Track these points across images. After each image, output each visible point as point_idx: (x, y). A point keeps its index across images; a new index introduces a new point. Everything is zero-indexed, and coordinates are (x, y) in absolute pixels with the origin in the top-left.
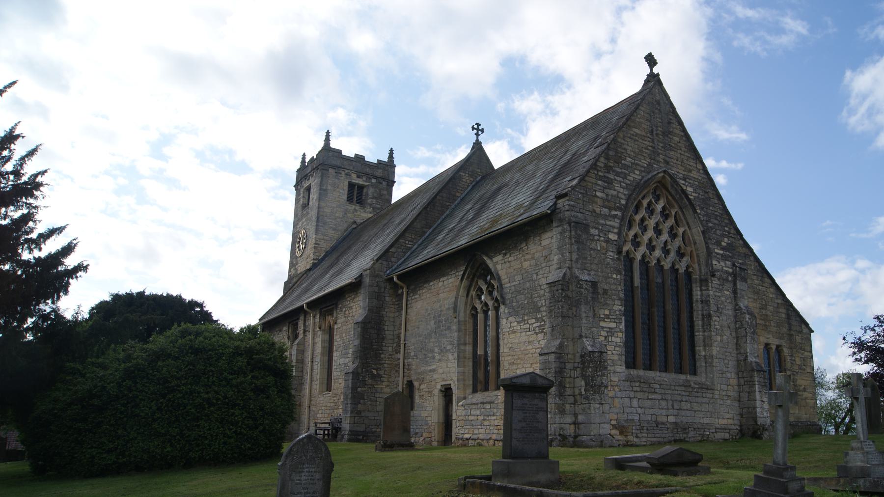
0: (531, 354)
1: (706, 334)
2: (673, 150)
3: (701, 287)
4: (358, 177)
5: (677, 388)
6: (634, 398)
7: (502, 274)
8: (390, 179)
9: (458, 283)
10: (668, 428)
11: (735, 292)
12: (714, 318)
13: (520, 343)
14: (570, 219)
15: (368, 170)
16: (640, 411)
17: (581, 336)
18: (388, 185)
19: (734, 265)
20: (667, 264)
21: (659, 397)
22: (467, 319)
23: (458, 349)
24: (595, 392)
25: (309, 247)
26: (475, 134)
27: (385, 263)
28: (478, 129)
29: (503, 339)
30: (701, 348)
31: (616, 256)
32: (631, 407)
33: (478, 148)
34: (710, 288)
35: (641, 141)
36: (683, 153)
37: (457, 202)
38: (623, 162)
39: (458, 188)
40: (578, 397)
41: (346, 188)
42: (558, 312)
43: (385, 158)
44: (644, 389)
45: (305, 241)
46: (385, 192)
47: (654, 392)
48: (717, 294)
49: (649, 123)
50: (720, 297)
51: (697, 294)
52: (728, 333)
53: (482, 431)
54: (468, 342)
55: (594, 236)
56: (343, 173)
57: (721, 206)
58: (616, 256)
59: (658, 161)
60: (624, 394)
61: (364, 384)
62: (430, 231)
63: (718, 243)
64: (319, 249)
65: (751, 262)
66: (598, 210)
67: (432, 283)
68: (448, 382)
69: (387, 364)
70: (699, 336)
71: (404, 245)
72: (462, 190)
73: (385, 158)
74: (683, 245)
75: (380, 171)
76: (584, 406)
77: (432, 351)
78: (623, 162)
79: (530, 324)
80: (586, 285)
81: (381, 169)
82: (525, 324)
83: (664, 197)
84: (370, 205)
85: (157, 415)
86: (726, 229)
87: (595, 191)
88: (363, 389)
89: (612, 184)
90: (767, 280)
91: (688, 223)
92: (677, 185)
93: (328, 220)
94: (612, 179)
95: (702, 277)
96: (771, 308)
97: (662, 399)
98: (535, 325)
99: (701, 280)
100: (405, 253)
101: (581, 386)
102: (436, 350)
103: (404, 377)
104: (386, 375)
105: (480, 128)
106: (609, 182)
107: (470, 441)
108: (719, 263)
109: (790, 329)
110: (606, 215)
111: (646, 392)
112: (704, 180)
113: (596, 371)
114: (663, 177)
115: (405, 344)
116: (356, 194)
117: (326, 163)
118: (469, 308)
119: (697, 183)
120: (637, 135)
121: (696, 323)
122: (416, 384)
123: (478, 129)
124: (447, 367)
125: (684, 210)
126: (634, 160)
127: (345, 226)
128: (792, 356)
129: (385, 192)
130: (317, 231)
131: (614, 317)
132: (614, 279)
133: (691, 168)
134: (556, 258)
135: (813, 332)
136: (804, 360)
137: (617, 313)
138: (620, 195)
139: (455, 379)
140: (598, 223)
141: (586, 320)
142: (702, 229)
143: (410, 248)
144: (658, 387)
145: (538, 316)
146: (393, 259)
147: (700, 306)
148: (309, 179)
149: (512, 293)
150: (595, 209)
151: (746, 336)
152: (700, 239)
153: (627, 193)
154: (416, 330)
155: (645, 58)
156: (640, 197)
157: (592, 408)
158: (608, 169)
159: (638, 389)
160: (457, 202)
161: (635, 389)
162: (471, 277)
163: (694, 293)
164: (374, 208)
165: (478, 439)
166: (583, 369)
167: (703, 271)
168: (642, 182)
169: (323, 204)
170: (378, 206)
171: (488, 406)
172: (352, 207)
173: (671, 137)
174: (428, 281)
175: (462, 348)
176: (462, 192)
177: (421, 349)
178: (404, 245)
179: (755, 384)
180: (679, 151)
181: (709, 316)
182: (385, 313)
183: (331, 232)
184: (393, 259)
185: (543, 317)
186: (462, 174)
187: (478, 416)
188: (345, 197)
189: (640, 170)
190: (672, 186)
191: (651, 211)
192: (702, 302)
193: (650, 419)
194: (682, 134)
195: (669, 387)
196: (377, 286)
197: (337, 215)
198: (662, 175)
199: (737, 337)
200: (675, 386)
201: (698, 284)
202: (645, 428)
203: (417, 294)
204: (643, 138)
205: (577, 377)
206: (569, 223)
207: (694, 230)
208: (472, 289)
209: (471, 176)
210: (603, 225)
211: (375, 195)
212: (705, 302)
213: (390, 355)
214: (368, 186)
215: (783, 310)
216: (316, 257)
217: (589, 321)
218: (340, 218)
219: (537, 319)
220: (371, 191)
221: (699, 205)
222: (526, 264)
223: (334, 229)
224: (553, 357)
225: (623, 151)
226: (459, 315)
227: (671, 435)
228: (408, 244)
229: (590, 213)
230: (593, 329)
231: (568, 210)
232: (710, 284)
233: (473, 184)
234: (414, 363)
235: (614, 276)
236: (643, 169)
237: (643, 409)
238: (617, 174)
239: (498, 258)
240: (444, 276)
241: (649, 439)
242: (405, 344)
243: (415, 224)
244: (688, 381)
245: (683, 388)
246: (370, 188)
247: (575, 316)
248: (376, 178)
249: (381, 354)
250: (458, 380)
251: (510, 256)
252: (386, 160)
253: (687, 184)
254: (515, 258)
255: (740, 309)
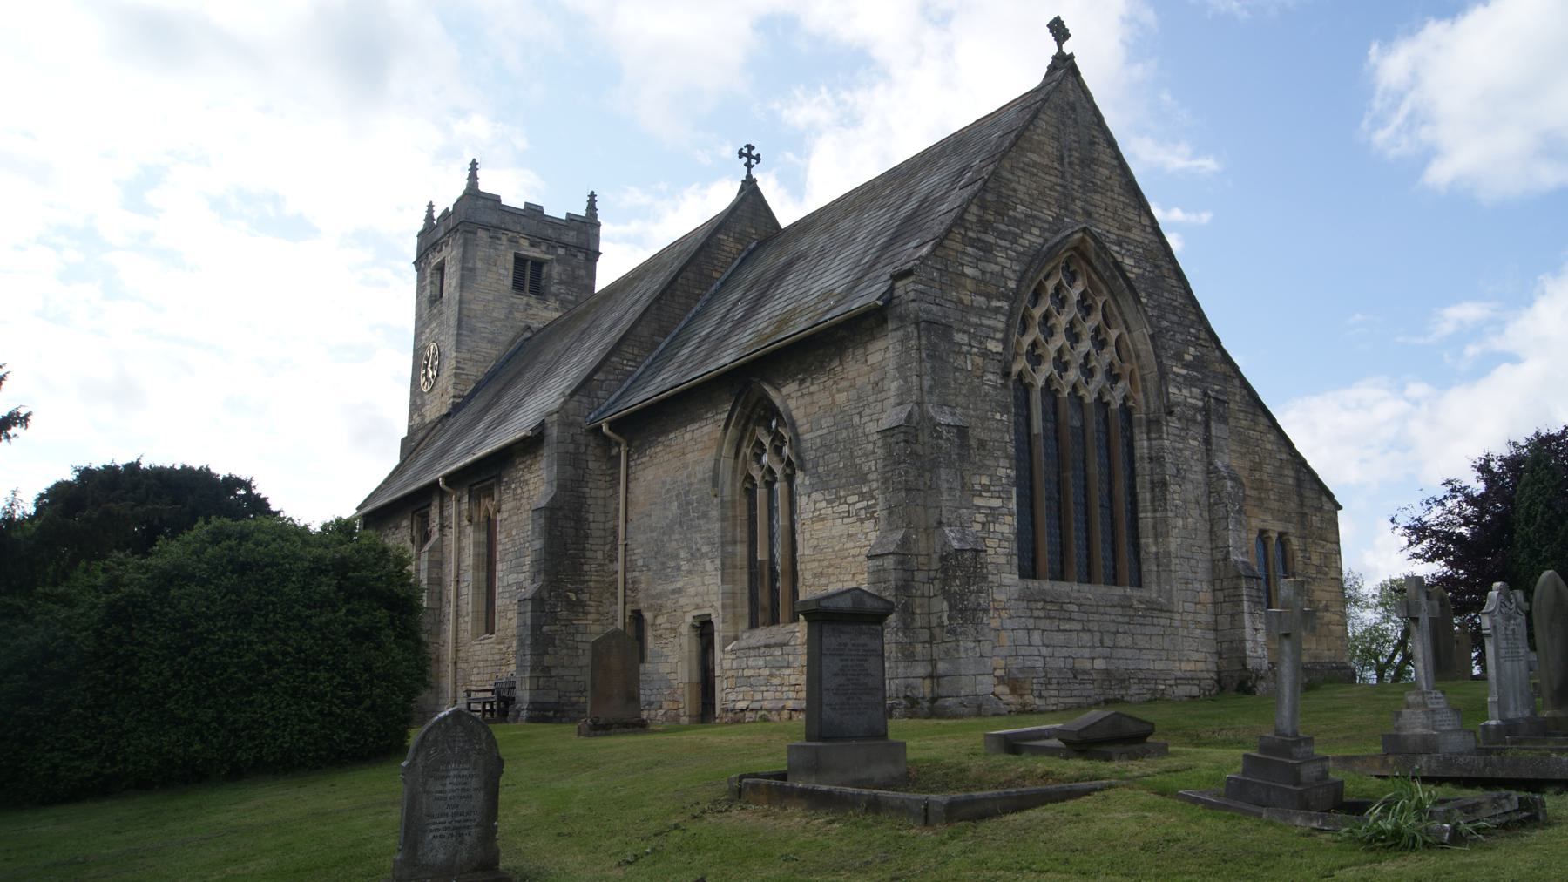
0: (853, 556)
1: (1158, 515)
2: (1099, 192)
3: (1148, 433)
4: (532, 245)
5: (1108, 610)
6: (1035, 629)
7: (798, 415)
8: (592, 248)
9: (719, 434)
10: (1093, 680)
11: (1207, 441)
12: (1172, 488)
13: (833, 538)
14: (917, 317)
15: (550, 232)
16: (1044, 651)
17: (940, 523)
18: (587, 259)
19: (1205, 394)
20: (1089, 395)
21: (1078, 626)
22: (737, 497)
23: (722, 551)
24: (965, 621)
25: (445, 375)
26: (745, 165)
27: (585, 400)
28: (749, 156)
29: (803, 532)
30: (1150, 540)
31: (999, 381)
32: (1030, 645)
33: (750, 190)
34: (1165, 436)
35: (1043, 175)
36: (1116, 196)
37: (713, 288)
38: (1011, 213)
39: (715, 262)
40: (937, 631)
41: (511, 266)
42: (900, 482)
43: (581, 211)
44: (1052, 614)
45: (437, 363)
46: (582, 272)
47: (1070, 619)
48: (1177, 445)
49: (1056, 144)
50: (1181, 450)
51: (1142, 445)
52: (1195, 512)
53: (768, 695)
54: (739, 539)
55: (961, 345)
56: (504, 238)
57: (1182, 291)
58: (999, 381)
59: (1073, 212)
60: (1016, 623)
61: (554, 618)
62: (667, 340)
63: (1178, 357)
64: (463, 376)
65: (1234, 388)
66: (967, 300)
67: (672, 435)
68: (706, 611)
69: (595, 581)
70: (1146, 518)
71: (620, 367)
72: (722, 267)
73: (581, 211)
74: (1116, 361)
75: (572, 233)
76: (948, 645)
77: (676, 557)
78: (1011, 213)
79: (849, 505)
80: (948, 432)
81: (573, 229)
82: (840, 504)
83: (1083, 275)
84: (556, 296)
85: (173, 686)
86: (1192, 330)
87: (962, 265)
88: (553, 628)
89: (991, 253)
90: (1264, 420)
91: (1125, 322)
92: (1106, 254)
93: (479, 325)
94: (991, 244)
95: (1151, 416)
96: (1269, 469)
97: (1083, 630)
98: (859, 506)
99: (1149, 422)
100: (622, 381)
101: (942, 611)
102: (683, 554)
103: (625, 604)
104: (594, 601)
105: (754, 153)
106: (988, 249)
107: (748, 714)
108: (1180, 390)
109: (1302, 505)
110: (982, 309)
111: (1054, 618)
112: (1154, 245)
113: (968, 583)
114: (1083, 240)
115: (626, 545)
116: (528, 277)
117: (473, 220)
118: (740, 478)
119: (1141, 250)
120: (1035, 164)
121: (1140, 497)
122: (648, 616)
123: (749, 156)
124: (704, 584)
125: (1119, 300)
126: (1031, 209)
127: (511, 334)
128: (1305, 550)
129: (582, 272)
130: (459, 344)
131: (997, 489)
132: (998, 421)
133: (1131, 223)
134: (894, 385)
135: (1340, 508)
136: (1326, 557)
137: (1004, 481)
138: (1006, 272)
139: (718, 604)
140: (968, 323)
141: (949, 495)
142: (1151, 332)
143: (631, 373)
144: (1075, 608)
145: (864, 490)
146: (600, 394)
147: (1147, 465)
148: (441, 250)
149: (816, 450)
150: (963, 297)
151: (1227, 518)
152: (1146, 348)
153: (1017, 268)
154: (645, 519)
155: (1048, 26)
156: (1042, 276)
157: (962, 649)
158: (985, 225)
159: (1042, 614)
160: (713, 288)
161: (1036, 613)
162: (743, 422)
163: (1137, 444)
164: (563, 302)
165: (761, 709)
166: (944, 582)
167: (1152, 406)
168: (1045, 248)
169: (467, 295)
170: (571, 298)
171: (778, 652)
172: (521, 300)
173: (1096, 167)
174: (665, 432)
175: (730, 549)
176: (723, 270)
177: (656, 553)
178: (620, 367)
179: (1242, 601)
180: (1109, 194)
181: (1164, 485)
182: (588, 490)
183: (484, 347)
184: (600, 394)
185: (872, 491)
186: (722, 237)
187: (760, 669)
188: (509, 282)
189: (1040, 228)
190: (1098, 256)
191: (1060, 300)
192: (1151, 459)
193: (1062, 666)
194: (1115, 162)
195: (1094, 610)
196: (573, 441)
197: (495, 315)
198: (1080, 235)
199: (1212, 521)
200: (1105, 606)
201: (1144, 429)
202: (1054, 681)
203: (645, 456)
204: (1046, 170)
205: (935, 596)
206: (917, 324)
207: (1136, 334)
208: (745, 443)
209: (738, 241)
210: (976, 326)
211: (564, 277)
212: (1156, 459)
213: (600, 565)
214: (551, 260)
215: (1289, 472)
216: (457, 393)
217: (955, 496)
218: (499, 320)
219: (862, 496)
220: (556, 271)
221: (1145, 290)
222: (841, 398)
223: (490, 341)
224: (892, 561)
225: (1012, 193)
226: (722, 491)
227: (1098, 691)
228: (627, 365)
229: (953, 306)
230: (962, 511)
231: (913, 300)
232: (1165, 428)
233: (743, 255)
234: (643, 578)
235: (998, 416)
236: (1046, 226)
237: (1050, 649)
238: (1001, 235)
239: (791, 388)
240: (693, 421)
241: (1061, 700)
242: (626, 545)
243: (639, 328)
244: (1129, 598)
245: (1120, 611)
246: (555, 264)
247: (930, 488)
248: (566, 246)
249: (582, 564)
250: (724, 607)
251: (812, 384)
252: (583, 214)
253: (1123, 252)
254: (822, 387)
255: (1217, 470)
